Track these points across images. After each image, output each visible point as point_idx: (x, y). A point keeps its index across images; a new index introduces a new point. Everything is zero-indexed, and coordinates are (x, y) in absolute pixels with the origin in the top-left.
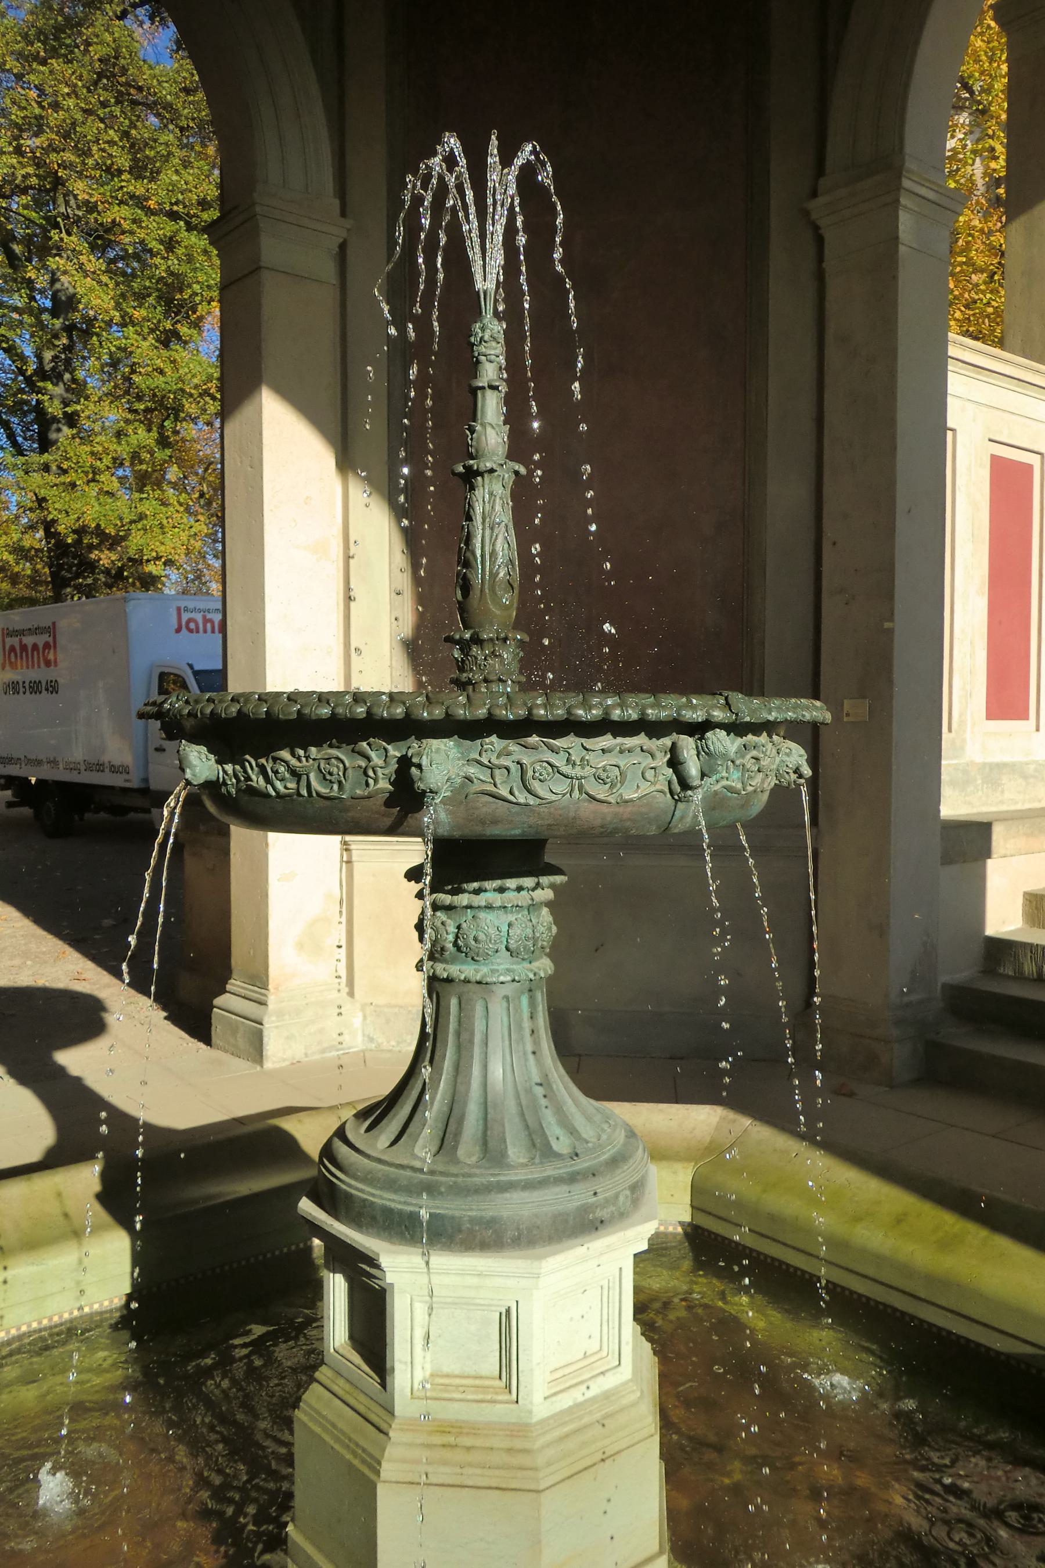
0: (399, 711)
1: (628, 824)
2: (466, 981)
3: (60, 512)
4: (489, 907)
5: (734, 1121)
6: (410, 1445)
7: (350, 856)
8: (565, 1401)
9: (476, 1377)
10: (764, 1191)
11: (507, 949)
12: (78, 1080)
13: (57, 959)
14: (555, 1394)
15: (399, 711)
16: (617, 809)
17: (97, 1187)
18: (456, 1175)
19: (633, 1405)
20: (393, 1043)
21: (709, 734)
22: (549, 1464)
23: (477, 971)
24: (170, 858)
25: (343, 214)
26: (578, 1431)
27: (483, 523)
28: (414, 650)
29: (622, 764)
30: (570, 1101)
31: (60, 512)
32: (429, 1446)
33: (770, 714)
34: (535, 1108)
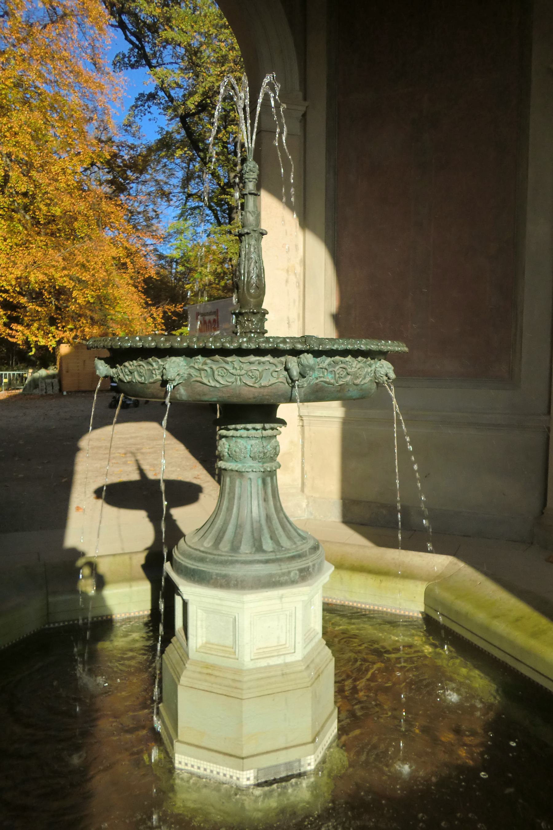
0: (153, 344)
1: (267, 397)
2: (232, 470)
3: (233, 254)
4: (241, 437)
5: (456, 564)
6: (194, 672)
7: (303, 423)
8: (263, 663)
9: (223, 646)
10: (456, 599)
11: (250, 457)
12: (175, 521)
13: (191, 469)
14: (257, 659)
15: (153, 344)
16: (260, 390)
17: (143, 561)
18: (215, 555)
19: (301, 672)
20: (322, 516)
21: (301, 356)
22: (249, 688)
23: (236, 466)
24: (394, 440)
25: (305, 99)
26: (269, 677)
27: (245, 258)
28: (337, 319)
29: (260, 370)
30: (280, 529)
31: (233, 254)
32: (200, 673)
33: (334, 346)
34: (260, 529)
